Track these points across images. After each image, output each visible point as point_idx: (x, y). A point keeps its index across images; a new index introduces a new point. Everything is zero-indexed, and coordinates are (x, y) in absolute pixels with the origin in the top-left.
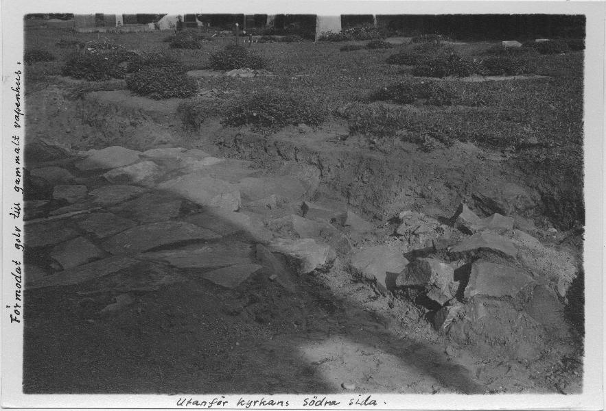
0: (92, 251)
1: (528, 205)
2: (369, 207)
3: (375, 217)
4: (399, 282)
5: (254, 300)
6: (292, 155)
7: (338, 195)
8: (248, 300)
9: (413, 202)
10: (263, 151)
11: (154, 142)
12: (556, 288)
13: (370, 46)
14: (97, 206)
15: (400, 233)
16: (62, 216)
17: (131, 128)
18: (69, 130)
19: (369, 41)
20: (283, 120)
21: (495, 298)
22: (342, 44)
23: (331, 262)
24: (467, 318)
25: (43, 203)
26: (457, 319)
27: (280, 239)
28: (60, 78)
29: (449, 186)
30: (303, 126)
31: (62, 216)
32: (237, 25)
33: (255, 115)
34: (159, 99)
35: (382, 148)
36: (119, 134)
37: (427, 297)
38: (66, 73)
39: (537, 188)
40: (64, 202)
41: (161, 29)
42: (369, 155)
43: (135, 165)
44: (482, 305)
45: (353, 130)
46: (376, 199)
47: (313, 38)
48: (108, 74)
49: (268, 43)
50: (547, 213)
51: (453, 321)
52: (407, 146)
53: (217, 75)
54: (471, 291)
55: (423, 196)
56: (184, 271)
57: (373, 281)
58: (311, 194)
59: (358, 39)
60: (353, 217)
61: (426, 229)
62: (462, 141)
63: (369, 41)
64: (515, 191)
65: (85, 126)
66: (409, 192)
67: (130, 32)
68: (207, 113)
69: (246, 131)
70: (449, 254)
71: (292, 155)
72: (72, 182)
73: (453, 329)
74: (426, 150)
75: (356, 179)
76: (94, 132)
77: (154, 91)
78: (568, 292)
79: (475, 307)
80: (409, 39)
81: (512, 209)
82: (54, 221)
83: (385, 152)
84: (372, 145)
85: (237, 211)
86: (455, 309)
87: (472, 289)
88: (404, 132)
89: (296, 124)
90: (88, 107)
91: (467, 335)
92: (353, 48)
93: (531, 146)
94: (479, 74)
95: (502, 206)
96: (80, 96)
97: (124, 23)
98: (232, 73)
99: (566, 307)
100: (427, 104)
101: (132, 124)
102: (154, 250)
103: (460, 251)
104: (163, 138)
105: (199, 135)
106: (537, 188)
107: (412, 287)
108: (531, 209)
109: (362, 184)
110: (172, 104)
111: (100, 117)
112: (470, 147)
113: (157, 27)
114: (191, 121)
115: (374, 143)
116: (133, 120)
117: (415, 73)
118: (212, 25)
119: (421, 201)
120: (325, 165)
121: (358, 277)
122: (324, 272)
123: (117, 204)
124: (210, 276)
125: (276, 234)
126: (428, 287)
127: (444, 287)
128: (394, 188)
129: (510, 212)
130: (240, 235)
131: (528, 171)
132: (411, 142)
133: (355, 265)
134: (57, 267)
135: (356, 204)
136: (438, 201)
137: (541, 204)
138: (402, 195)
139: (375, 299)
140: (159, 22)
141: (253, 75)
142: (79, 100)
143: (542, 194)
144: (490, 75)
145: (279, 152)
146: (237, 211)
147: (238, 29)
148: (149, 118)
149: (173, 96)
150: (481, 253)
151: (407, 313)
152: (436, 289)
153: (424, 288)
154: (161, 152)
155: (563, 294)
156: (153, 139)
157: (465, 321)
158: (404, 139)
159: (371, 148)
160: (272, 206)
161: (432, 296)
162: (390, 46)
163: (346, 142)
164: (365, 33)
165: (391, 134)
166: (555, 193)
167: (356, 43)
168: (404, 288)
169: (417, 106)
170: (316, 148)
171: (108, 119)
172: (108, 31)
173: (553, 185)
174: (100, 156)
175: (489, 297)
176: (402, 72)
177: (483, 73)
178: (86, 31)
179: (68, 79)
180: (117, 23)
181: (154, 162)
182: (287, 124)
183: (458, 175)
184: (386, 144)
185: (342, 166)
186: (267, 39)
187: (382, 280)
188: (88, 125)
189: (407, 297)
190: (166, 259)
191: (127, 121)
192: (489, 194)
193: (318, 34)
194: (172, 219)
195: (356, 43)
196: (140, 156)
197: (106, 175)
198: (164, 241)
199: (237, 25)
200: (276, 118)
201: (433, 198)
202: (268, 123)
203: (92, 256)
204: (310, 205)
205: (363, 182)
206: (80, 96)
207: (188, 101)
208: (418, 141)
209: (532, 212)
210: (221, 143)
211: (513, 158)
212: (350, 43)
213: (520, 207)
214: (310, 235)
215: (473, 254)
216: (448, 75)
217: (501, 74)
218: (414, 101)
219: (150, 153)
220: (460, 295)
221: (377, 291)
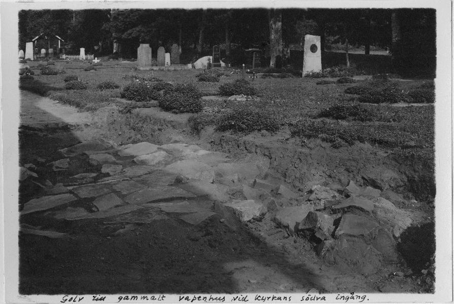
0: (118, 201)
1: (398, 184)
2: (297, 184)
3: (299, 190)
4: (300, 227)
5: (208, 234)
6: (253, 150)
7: (279, 175)
8: (204, 232)
9: (324, 180)
10: (237, 148)
11: (171, 141)
12: (393, 231)
13: (339, 82)
14: (127, 177)
15: (311, 199)
16: (105, 182)
17: (158, 132)
18: (120, 133)
19: (338, 78)
20: (250, 129)
21: (354, 236)
22: (319, 80)
23: (263, 215)
24: (336, 248)
25: (94, 175)
26: (330, 248)
27: (234, 200)
28: (118, 99)
29: (347, 170)
30: (264, 132)
31: (105, 182)
32: (244, 65)
33: (233, 123)
34: (177, 113)
35: (310, 146)
36: (151, 136)
37: (315, 236)
38: (123, 96)
39: (405, 173)
40: (108, 175)
41: (197, 68)
42: (300, 150)
43: (154, 154)
44: (345, 240)
45: (294, 134)
46: (301, 180)
47: (301, 77)
48: (150, 97)
49: (267, 79)
50: (411, 190)
51: (328, 250)
52: (324, 144)
53: (220, 99)
54: (339, 232)
55: (330, 176)
56: (168, 214)
57: (287, 227)
58: (263, 175)
59: (333, 76)
60: (283, 188)
61: (324, 193)
62: (361, 142)
63: (338, 78)
64: (388, 175)
65: (130, 131)
66: (322, 174)
67: (175, 70)
68: (206, 122)
69: (228, 134)
70: (332, 210)
71: (253, 150)
72: (115, 163)
73: (327, 255)
74: (335, 147)
75: (291, 165)
76: (136, 135)
77: (174, 108)
78: (402, 235)
79: (341, 242)
80: (370, 77)
81: (387, 186)
82: (100, 185)
83: (311, 149)
84: (303, 144)
85: (212, 183)
86: (329, 242)
87: (340, 230)
88: (324, 136)
89: (259, 130)
90: (133, 118)
91: (335, 258)
92: (326, 83)
93: (411, 147)
94: (405, 101)
95: (380, 184)
96: (129, 111)
97: (171, 64)
98: (232, 98)
99: (399, 244)
100: (355, 120)
101: (160, 130)
102: (154, 202)
103: (339, 208)
104: (177, 138)
105: (199, 137)
106: (405, 173)
107: (308, 230)
108: (401, 187)
109: (294, 169)
110: (183, 118)
111: (140, 125)
112: (367, 146)
113: (194, 67)
114: (196, 129)
115: (304, 142)
116: (160, 127)
117: (361, 100)
118: (232, 66)
119: (330, 181)
120: (273, 156)
121: (279, 225)
122: (258, 221)
123: (139, 176)
124: (183, 218)
125: (232, 197)
126: (316, 229)
127: (325, 230)
128: (313, 171)
129: (386, 188)
130: (205, 197)
131: (401, 162)
132: (327, 142)
133: (278, 217)
134: (96, 210)
135: (289, 181)
136: (340, 180)
137: (407, 184)
138: (317, 176)
139: (287, 238)
140: (195, 64)
141: (246, 99)
142: (128, 114)
143: (408, 177)
144: (414, 102)
145: (246, 147)
146: (212, 183)
147: (244, 68)
148: (169, 125)
149: (186, 112)
150: (351, 209)
151: (304, 246)
152: (320, 230)
153: (313, 230)
154: (171, 146)
155: (397, 235)
156: (171, 139)
157: (335, 250)
158: (323, 140)
159: (302, 146)
160: (235, 181)
161: (318, 235)
162: (354, 82)
163: (288, 142)
164: (338, 73)
165: (316, 137)
166: (416, 177)
167: (332, 80)
168: (302, 230)
169: (349, 121)
170: (269, 145)
171: (145, 126)
172: (160, 70)
173: (415, 171)
174: (130, 150)
175: (350, 236)
176: (353, 99)
177: (408, 101)
178: (145, 69)
179: (124, 101)
180: (166, 63)
181: (167, 152)
182: (254, 130)
183: (354, 163)
184: (312, 143)
185: (283, 157)
186: (266, 76)
187: (292, 227)
188: (133, 130)
189: (304, 237)
190: (159, 207)
191: (156, 128)
192: (372, 176)
193: (304, 73)
194: (169, 185)
195: (332, 80)
196: (158, 148)
197: (135, 159)
198: (161, 197)
199: (244, 65)
200: (247, 126)
201: (337, 178)
202: (242, 130)
203: (117, 204)
204: (258, 180)
205: (295, 167)
206: (129, 111)
207: (196, 115)
208: (331, 141)
209: (401, 189)
210: (212, 142)
211: (392, 154)
212: (326, 79)
213: (392, 185)
214: (253, 198)
215: (346, 210)
216: (382, 102)
217: (422, 102)
218: (346, 117)
219: (164, 146)
220: (333, 235)
221: (288, 232)
